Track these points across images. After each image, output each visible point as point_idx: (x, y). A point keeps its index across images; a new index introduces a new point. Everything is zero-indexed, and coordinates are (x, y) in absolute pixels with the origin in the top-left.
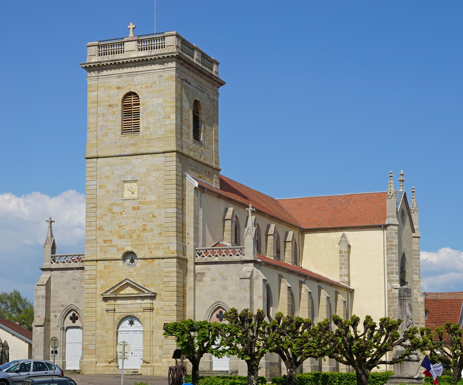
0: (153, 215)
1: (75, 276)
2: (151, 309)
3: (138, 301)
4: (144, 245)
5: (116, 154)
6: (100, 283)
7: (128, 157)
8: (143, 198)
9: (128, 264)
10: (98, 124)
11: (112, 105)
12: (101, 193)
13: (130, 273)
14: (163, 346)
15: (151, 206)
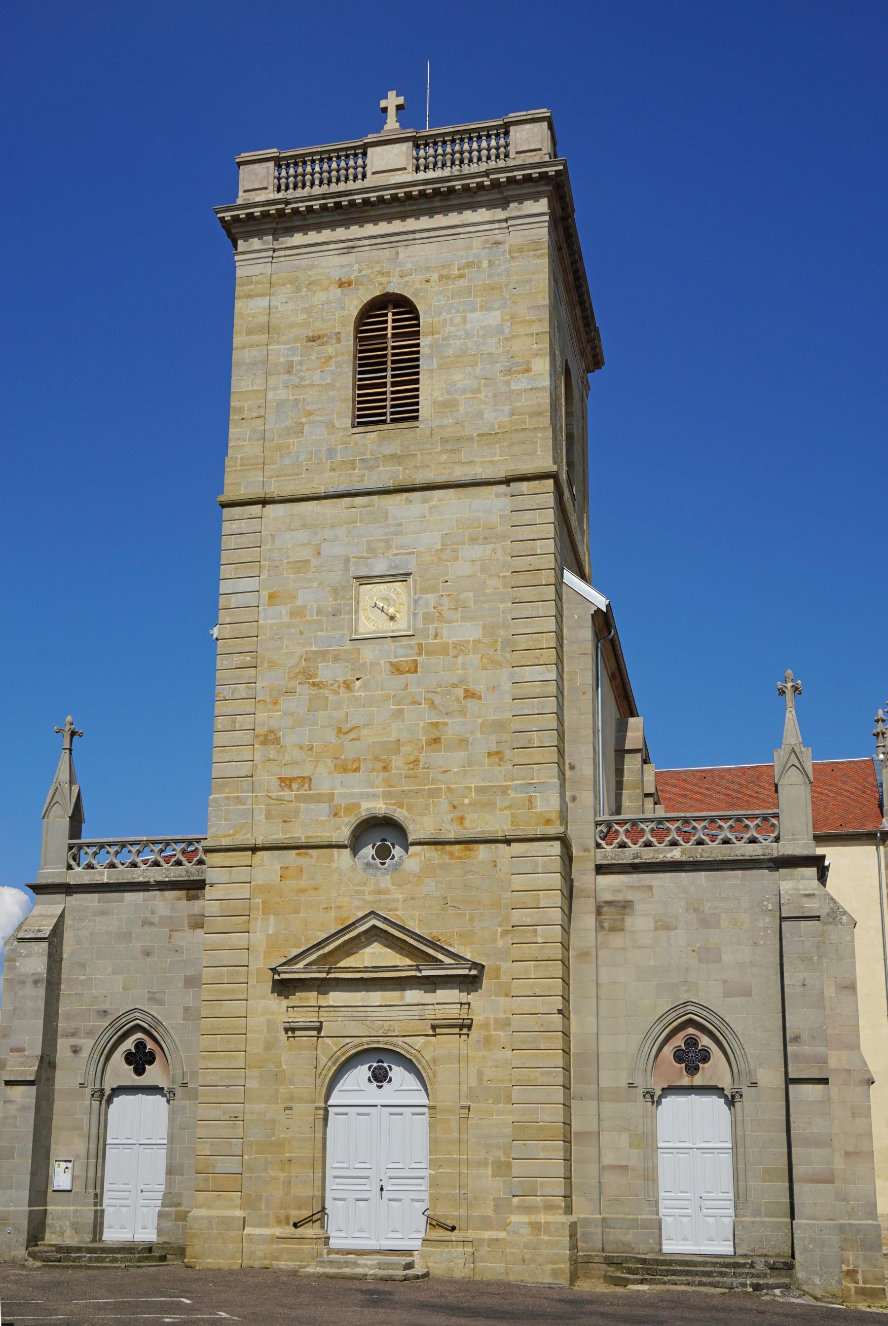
0: (466, 691)
1: (153, 913)
2: (461, 1027)
3: (413, 995)
4: (434, 793)
5: (332, 490)
6: (264, 929)
7: (376, 498)
8: (432, 632)
9: (368, 865)
10: (270, 395)
11: (319, 337)
12: (272, 617)
13: (379, 892)
14: (508, 1165)
15: (460, 660)
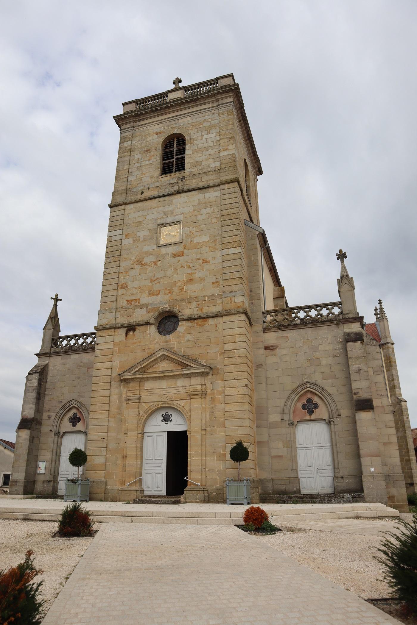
0: (203, 260)
2: (202, 394)
3: (180, 382)
